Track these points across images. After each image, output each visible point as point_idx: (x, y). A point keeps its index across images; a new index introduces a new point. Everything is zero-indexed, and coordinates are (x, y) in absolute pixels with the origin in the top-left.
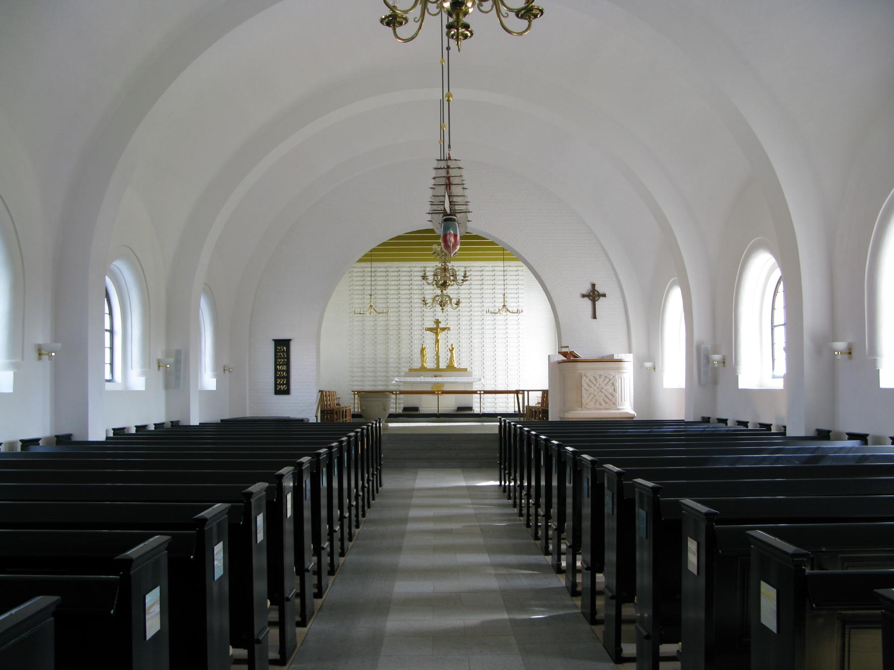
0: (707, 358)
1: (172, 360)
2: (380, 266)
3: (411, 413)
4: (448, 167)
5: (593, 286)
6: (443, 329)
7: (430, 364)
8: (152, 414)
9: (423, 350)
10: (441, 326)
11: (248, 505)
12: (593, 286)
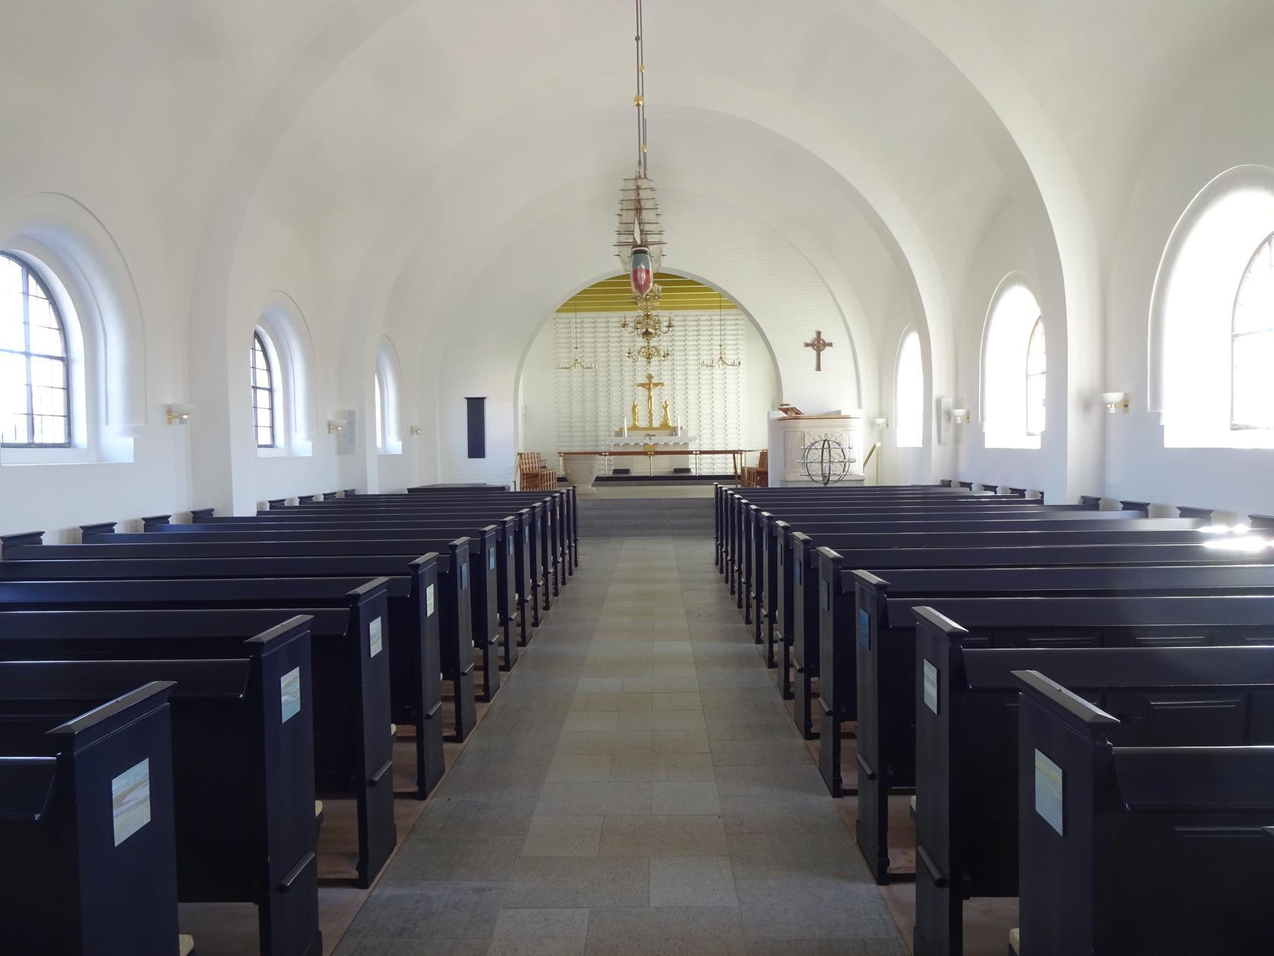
0: (949, 414)
1: (345, 422)
2: (587, 317)
3: (621, 477)
4: (638, 188)
5: (819, 333)
6: (656, 385)
7: (642, 423)
8: (322, 482)
9: (634, 407)
10: (654, 381)
11: (355, 612)
12: (819, 333)
